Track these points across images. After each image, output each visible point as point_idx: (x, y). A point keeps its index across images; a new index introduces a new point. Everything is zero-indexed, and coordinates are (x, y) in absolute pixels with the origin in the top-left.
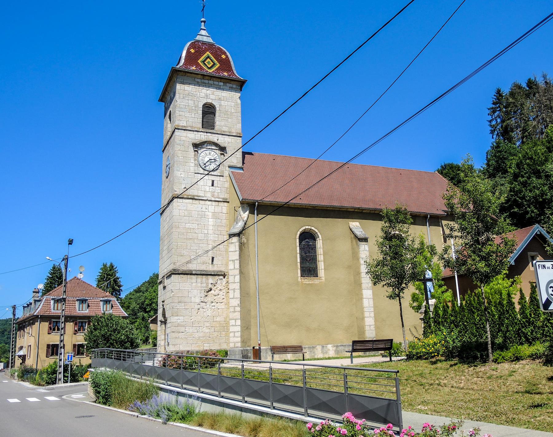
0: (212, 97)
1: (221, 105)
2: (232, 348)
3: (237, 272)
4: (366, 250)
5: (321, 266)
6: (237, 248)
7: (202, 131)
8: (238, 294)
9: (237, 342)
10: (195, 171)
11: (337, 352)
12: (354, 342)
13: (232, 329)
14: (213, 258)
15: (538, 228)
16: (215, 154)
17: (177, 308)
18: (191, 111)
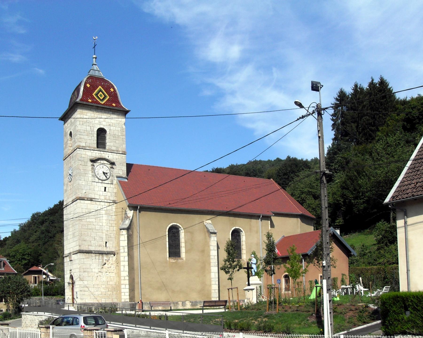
0: (104, 123)
1: (111, 130)
2: (124, 302)
3: (126, 254)
4: (215, 241)
5: (183, 250)
6: (126, 239)
7: (97, 150)
8: (127, 268)
9: (126, 299)
10: (92, 180)
11: (192, 305)
12: (204, 302)
13: (123, 290)
14: (106, 243)
15: (332, 229)
16: (107, 167)
17: (83, 275)
18: (89, 135)
